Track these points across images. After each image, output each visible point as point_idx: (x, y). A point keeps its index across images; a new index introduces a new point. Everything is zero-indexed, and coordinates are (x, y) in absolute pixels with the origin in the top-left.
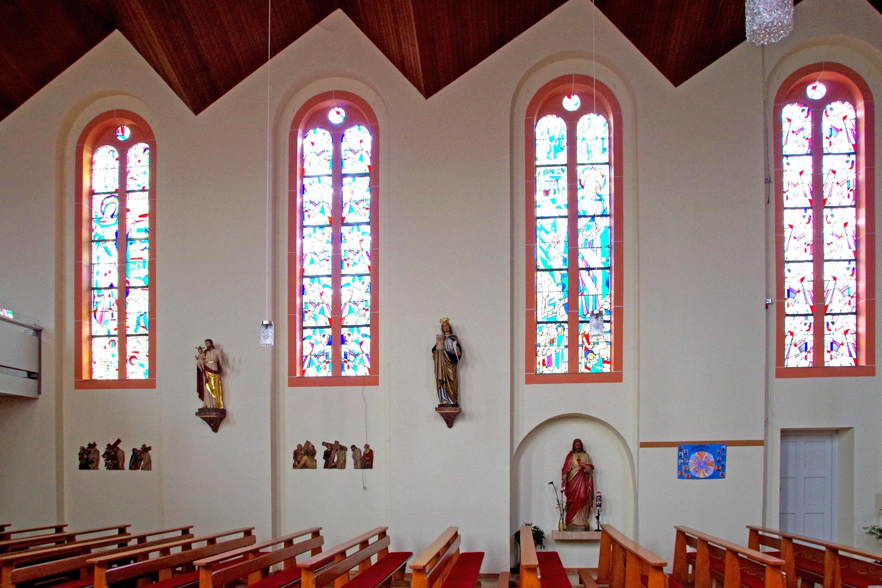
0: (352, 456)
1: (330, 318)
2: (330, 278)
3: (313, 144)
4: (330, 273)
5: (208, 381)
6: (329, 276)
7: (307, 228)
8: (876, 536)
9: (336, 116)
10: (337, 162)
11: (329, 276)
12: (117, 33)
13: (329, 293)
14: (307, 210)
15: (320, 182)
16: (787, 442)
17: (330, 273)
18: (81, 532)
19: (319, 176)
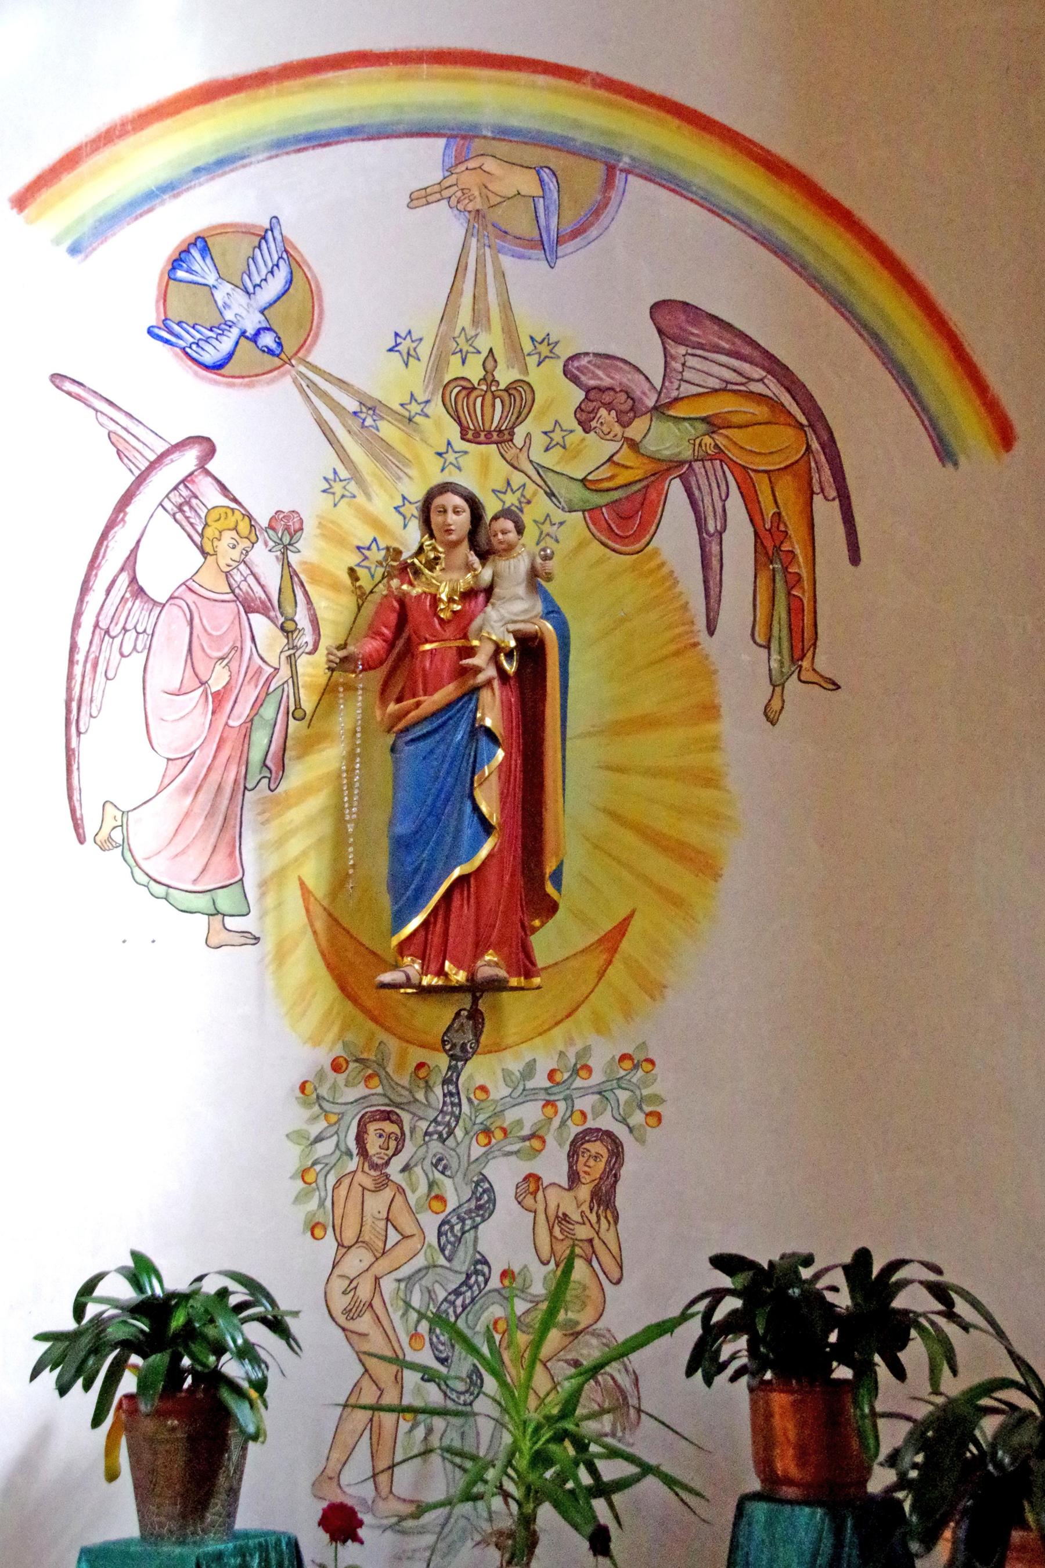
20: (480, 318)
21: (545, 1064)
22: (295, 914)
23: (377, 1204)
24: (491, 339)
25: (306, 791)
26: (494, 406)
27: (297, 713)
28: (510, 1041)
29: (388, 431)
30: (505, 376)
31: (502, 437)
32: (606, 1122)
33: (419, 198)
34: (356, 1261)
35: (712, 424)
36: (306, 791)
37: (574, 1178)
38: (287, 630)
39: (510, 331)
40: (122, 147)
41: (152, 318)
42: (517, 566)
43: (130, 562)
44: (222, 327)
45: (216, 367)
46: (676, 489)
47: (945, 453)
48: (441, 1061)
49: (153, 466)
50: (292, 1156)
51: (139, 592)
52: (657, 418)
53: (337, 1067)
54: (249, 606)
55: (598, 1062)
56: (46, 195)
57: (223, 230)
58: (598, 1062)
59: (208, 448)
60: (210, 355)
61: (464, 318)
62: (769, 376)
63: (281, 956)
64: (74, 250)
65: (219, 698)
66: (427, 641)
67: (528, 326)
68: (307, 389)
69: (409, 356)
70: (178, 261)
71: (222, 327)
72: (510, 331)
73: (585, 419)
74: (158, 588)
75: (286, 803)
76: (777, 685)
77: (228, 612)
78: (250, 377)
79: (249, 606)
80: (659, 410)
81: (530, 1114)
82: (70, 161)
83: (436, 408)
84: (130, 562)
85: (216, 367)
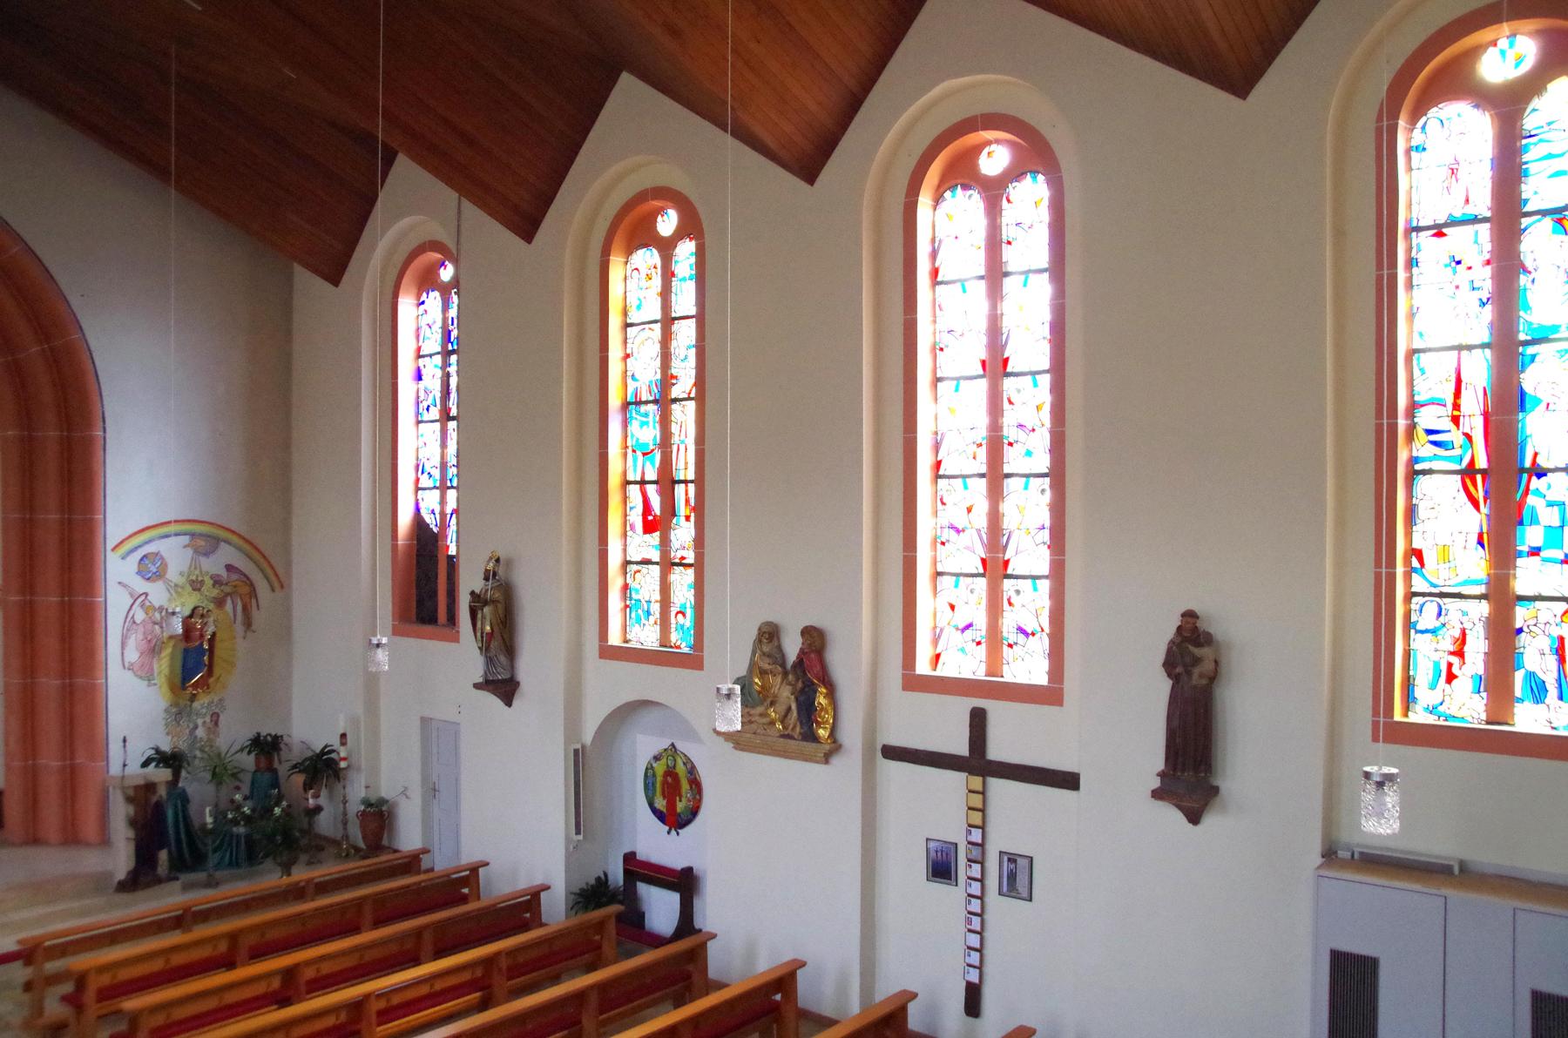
0: (1164, 665)
1: (984, 557)
2: (984, 480)
3: (952, 607)
4: (984, 469)
5: (683, 558)
6: (982, 476)
7: (944, 382)
8: (153, 764)
9: (995, 160)
10: (994, 244)
11: (982, 476)
12: (626, 80)
13: (982, 506)
14: (944, 541)
15: (966, 487)
16: (572, 908)
17: (984, 469)
18: (1033, 893)
19: (964, 477)
20: (195, 568)
21: (206, 701)
22: (163, 680)
23: (178, 729)
24: (197, 572)
25: (165, 657)
26: (625, 499)
27: (163, 643)
28: (172, 643)
29: (180, 590)
30: (200, 579)
31: (199, 590)
32: (217, 711)
33: (185, 547)
34: (175, 739)
35: (235, 587)
36: (165, 657)
37: (211, 721)
38: (162, 627)
39: (201, 572)
40: (130, 539)
41: (136, 571)
42: (211, 619)
43: (133, 617)
44: (149, 572)
45: (148, 579)
46: (229, 598)
47: (273, 590)
48: (189, 703)
49: (137, 598)
50: (163, 722)
51: (134, 622)
52: (1407, 424)
53: (171, 705)
54: (155, 623)
55: (215, 700)
56: (117, 549)
57: (149, 554)
58: (215, 700)
59: (146, 594)
60: (147, 577)
61: (193, 567)
62: (691, 487)
63: (160, 687)
64: (123, 558)
65: (149, 641)
66: (202, 644)
67: (204, 569)
68: (164, 582)
69: (183, 576)
70: (142, 559)
71: (149, 572)
72: (201, 572)
73: (214, 586)
74: (138, 622)
75: (162, 659)
76: (245, 632)
77: (151, 625)
78: (154, 581)
79: (155, 623)
80: (226, 584)
81: (204, 711)
82: (122, 542)
83: (188, 585)
84: (133, 617)
85: (148, 579)
